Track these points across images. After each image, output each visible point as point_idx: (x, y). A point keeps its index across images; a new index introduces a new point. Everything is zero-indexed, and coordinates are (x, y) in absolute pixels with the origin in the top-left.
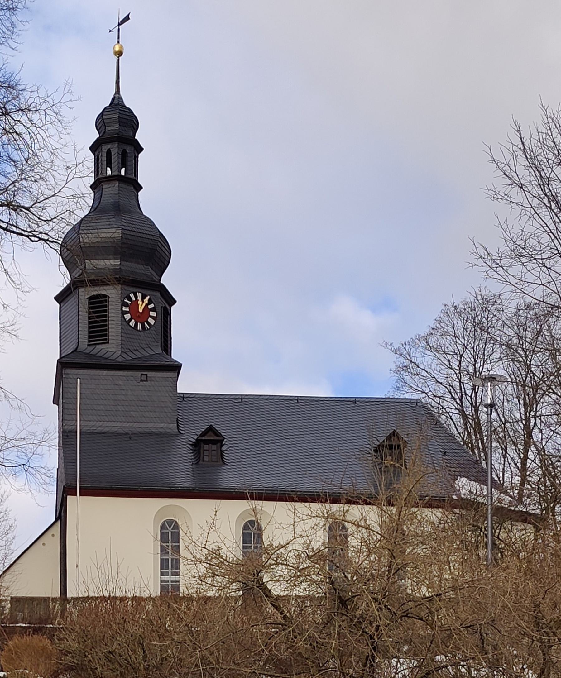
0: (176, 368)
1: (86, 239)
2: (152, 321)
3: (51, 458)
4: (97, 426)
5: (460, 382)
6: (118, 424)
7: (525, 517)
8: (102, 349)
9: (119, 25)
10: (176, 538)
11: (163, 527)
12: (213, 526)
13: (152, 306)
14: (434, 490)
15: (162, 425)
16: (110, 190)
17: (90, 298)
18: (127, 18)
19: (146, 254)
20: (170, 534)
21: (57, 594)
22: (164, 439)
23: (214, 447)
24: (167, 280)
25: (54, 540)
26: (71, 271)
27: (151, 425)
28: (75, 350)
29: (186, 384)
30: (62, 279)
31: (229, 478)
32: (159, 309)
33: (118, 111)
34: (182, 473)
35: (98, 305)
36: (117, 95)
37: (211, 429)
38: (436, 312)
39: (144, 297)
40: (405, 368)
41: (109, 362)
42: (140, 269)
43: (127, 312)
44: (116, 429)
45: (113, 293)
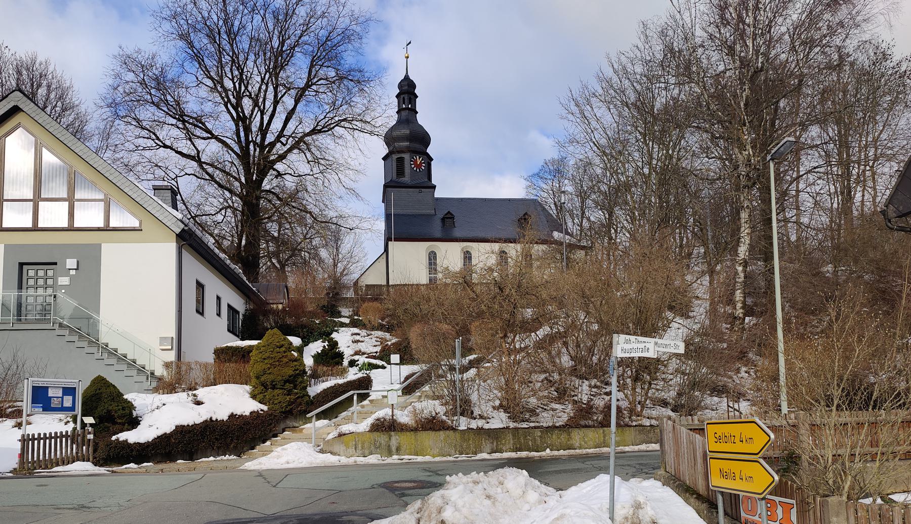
0: (434, 187)
1: (395, 134)
3: (381, 225)
4: (401, 212)
7: (583, 248)
8: (402, 179)
10: (435, 258)
12: (450, 255)
14: (543, 237)
16: (404, 113)
19: (421, 139)
21: (384, 283)
22: (429, 217)
24: (429, 150)
25: (383, 261)
29: (438, 194)
30: (385, 151)
31: (457, 233)
34: (437, 231)
40: (530, 186)
42: (417, 146)
45: (406, 156)
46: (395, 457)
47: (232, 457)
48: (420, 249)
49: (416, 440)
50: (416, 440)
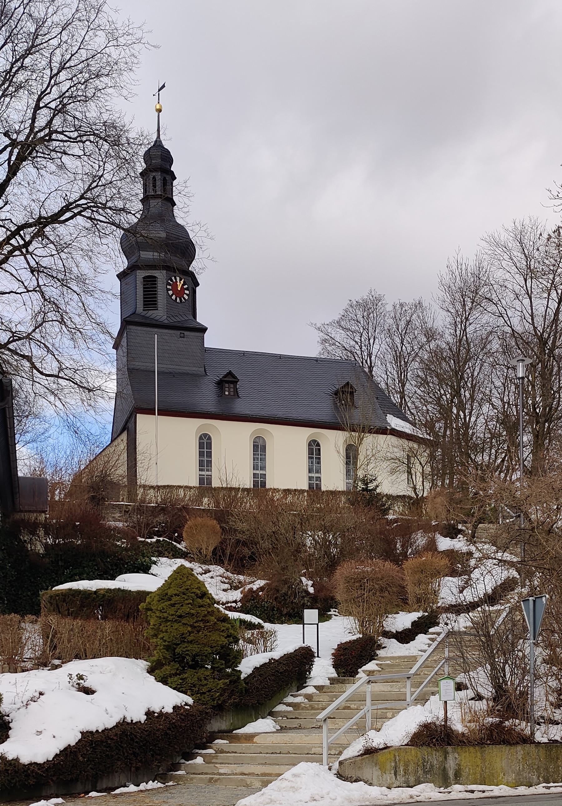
0: (204, 330)
2: (186, 297)
5: (361, 351)
6: (165, 366)
8: (152, 314)
9: (159, 91)
10: (209, 446)
11: (201, 438)
13: (186, 286)
15: (194, 369)
17: (144, 278)
18: (164, 86)
19: (179, 251)
20: (205, 444)
22: (195, 377)
23: (232, 386)
26: (129, 258)
27: (187, 368)
28: (134, 313)
30: (123, 263)
32: (190, 289)
33: (160, 150)
35: (150, 283)
36: (158, 139)
37: (230, 374)
38: (345, 305)
39: (180, 280)
41: (158, 323)
42: (176, 261)
43: (170, 290)
44: (163, 369)
45: (160, 275)
46: (458, 787)
47: (151, 785)
48: (188, 429)
49: (483, 760)
50: (483, 760)
